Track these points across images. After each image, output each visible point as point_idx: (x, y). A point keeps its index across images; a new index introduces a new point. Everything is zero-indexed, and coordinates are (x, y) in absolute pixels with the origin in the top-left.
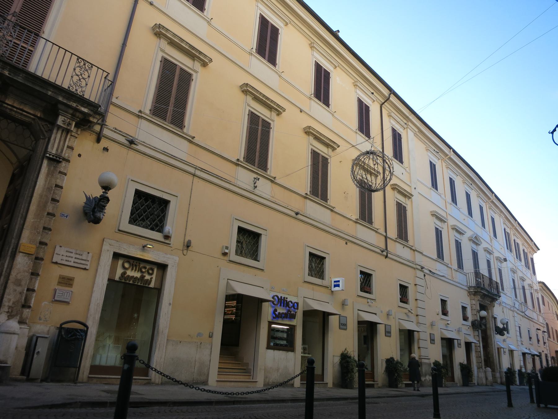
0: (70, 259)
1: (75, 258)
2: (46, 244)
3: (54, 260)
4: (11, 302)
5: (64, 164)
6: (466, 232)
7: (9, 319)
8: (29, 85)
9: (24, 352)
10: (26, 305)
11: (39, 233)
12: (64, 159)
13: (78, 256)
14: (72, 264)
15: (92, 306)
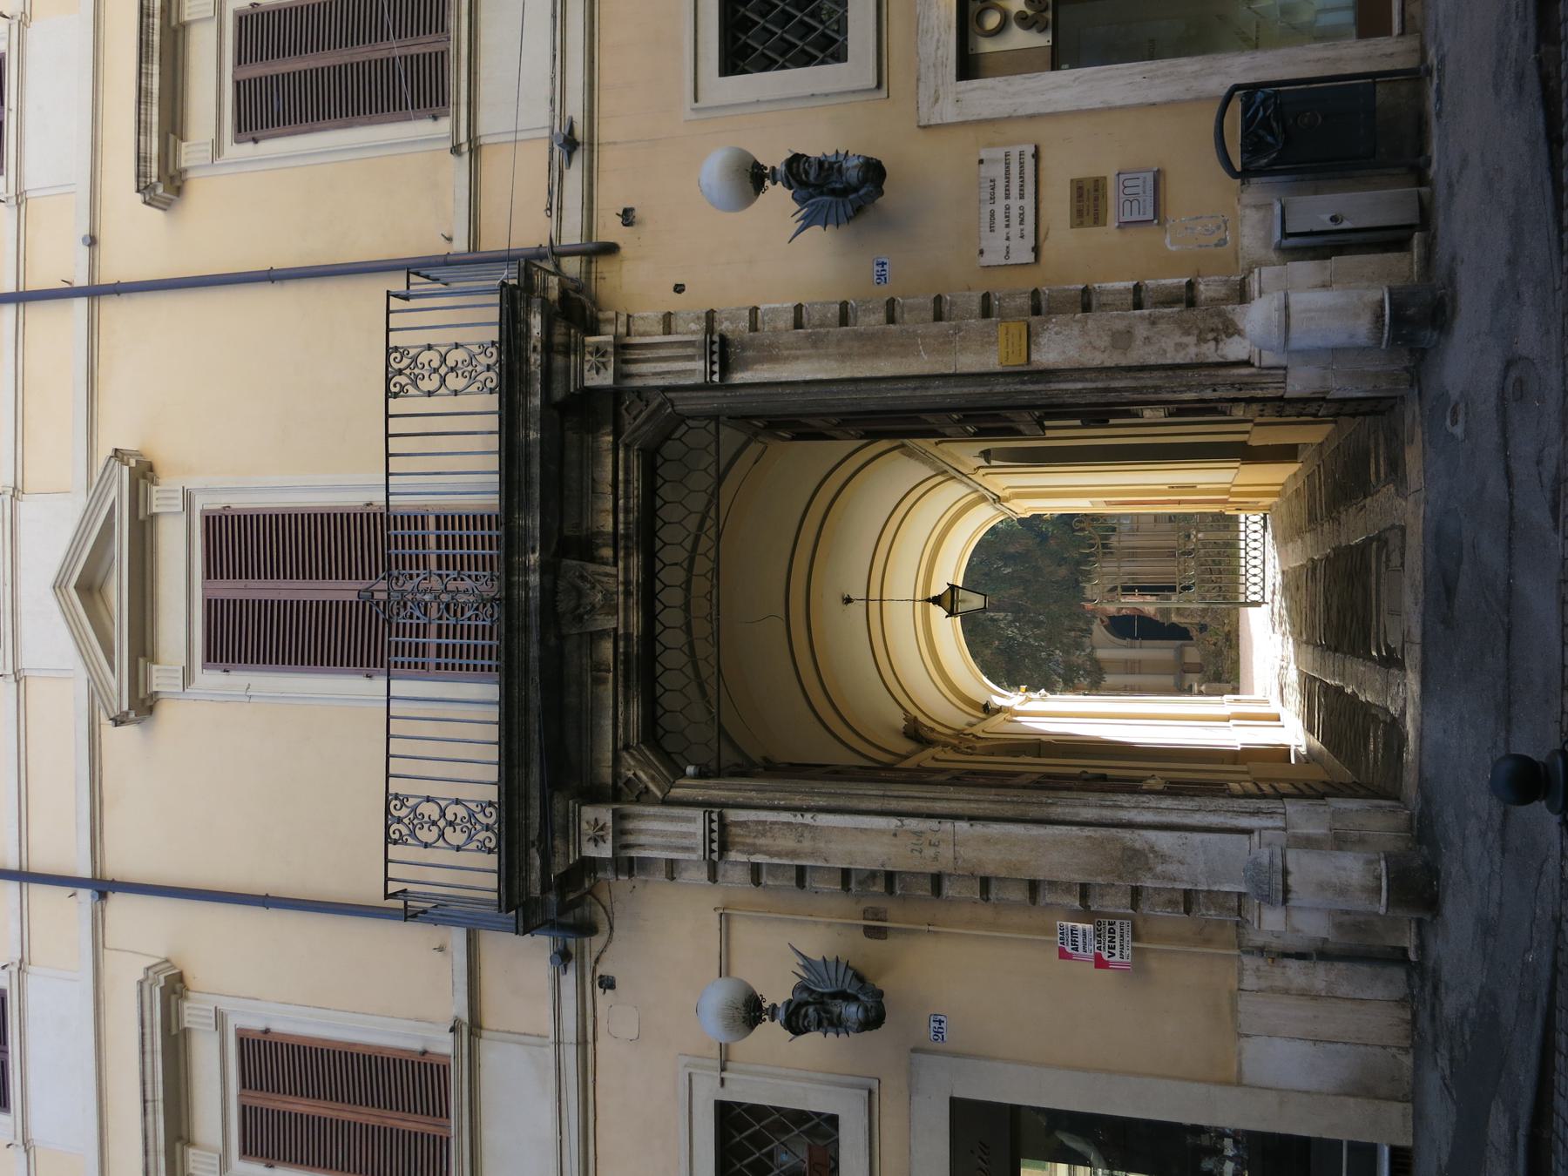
0: (1015, 213)
1: (1007, 197)
2: (986, 297)
3: (1030, 258)
4: (1185, 340)
5: (724, 326)
7: (1239, 332)
8: (537, 495)
9: (1335, 262)
10: (1188, 297)
11: (958, 329)
12: (710, 329)
13: (1000, 192)
14: (1029, 202)
15: (1156, 94)
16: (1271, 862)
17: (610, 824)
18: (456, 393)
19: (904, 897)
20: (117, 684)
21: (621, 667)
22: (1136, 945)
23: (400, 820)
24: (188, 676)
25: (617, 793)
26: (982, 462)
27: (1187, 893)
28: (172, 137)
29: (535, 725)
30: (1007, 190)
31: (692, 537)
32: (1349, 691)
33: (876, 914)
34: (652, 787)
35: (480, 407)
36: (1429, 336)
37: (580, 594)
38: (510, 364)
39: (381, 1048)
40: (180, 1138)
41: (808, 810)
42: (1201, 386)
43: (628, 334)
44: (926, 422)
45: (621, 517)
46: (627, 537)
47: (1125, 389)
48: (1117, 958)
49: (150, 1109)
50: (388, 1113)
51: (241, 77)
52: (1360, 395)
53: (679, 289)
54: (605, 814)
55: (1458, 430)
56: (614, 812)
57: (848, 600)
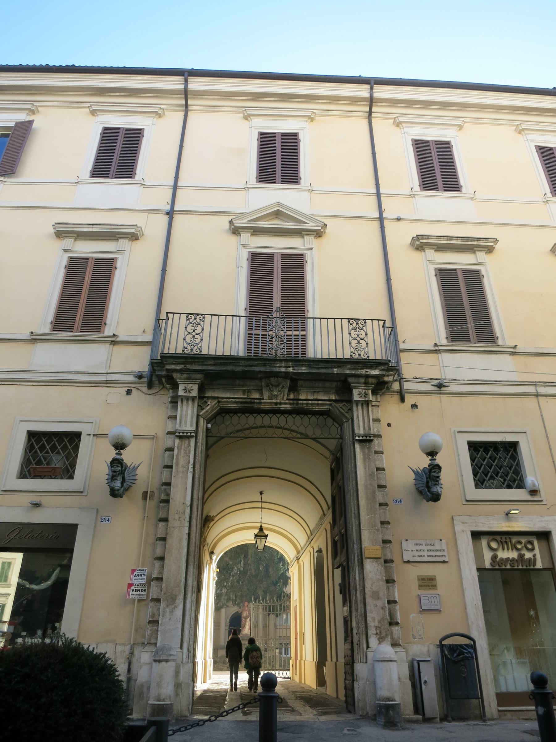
0: (422, 553)
1: (428, 550)
2: (390, 542)
3: (405, 560)
4: (376, 621)
5: (376, 441)
6: (496, 241)
7: (380, 643)
8: (314, 371)
9: (409, 684)
12: (375, 436)
13: (430, 548)
15: (470, 610)
16: (171, 655)
17: (191, 395)
18: (350, 343)
19: (158, 507)
20: (244, 222)
21: (249, 400)
22: (136, 601)
23: (195, 319)
25: (202, 397)
26: (316, 549)
28: (436, 247)
29: (229, 368)
30: (431, 550)
31: (288, 427)
32: (226, 703)
33: (152, 496)
34: (204, 411)
36: (382, 720)
37: (277, 386)
39: (108, 309)
40: (78, 236)
41: (194, 470)
42: (358, 628)
43: (372, 406)
45: (305, 402)
46: (297, 404)
48: (131, 592)
49: (90, 226)
50: (83, 310)
51: (458, 271)
52: (356, 695)
53: (389, 425)
54: (195, 393)
55: (345, 731)
56: (195, 397)
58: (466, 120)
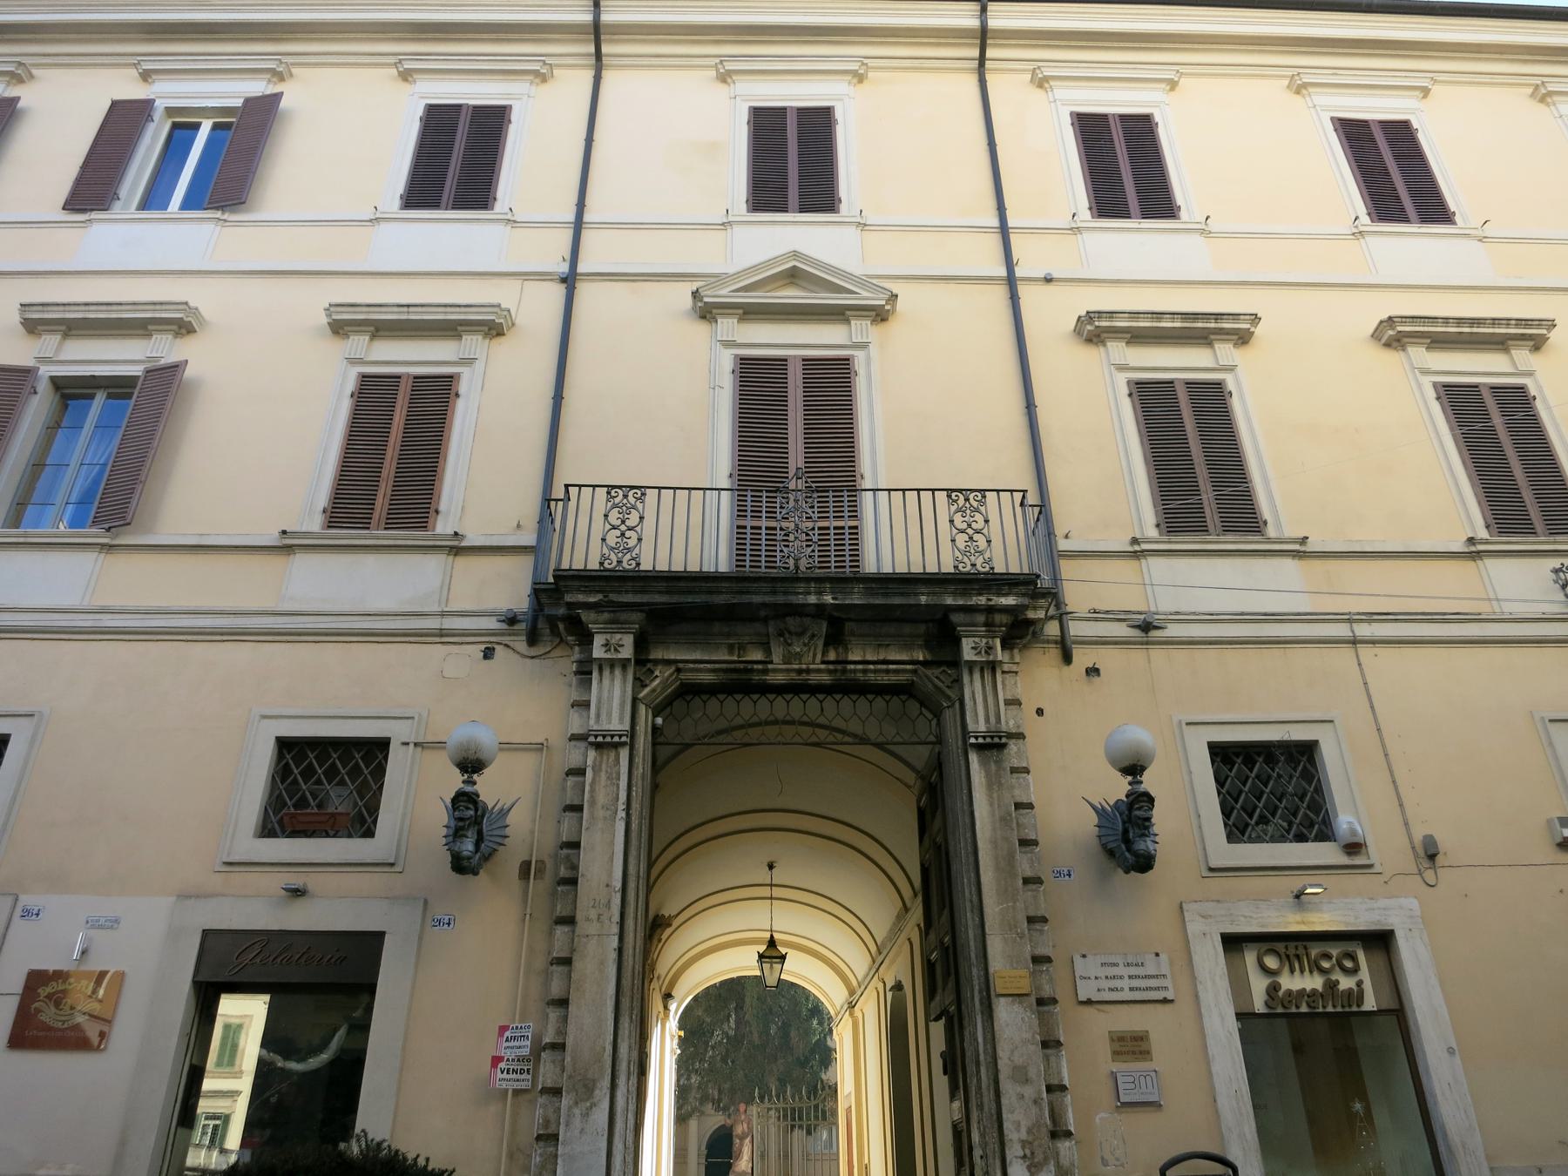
0: (1117, 983)
1: (1130, 977)
2: (1048, 960)
3: (1082, 998)
4: (1024, 1130)
5: (1013, 747)
11: (1022, 936)
12: (1010, 736)
13: (1134, 971)
14: (1127, 995)
15: (1224, 1103)
18: (953, 541)
19: (554, 894)
20: (724, 294)
23: (625, 496)
24: (728, 344)
25: (642, 662)
27: (555, 1137)
29: (698, 599)
30: (1137, 989)
33: (540, 871)
35: (945, 561)
37: (800, 634)
38: (978, 581)
40: (377, 330)
41: (628, 814)
42: (984, 1145)
44: (940, 915)
45: (860, 667)
46: (844, 671)
47: (979, 1080)
48: (500, 1075)
50: (391, 483)
53: (1040, 712)
54: (627, 652)
56: (629, 660)
57: (771, 867)
58: (1182, 69)
